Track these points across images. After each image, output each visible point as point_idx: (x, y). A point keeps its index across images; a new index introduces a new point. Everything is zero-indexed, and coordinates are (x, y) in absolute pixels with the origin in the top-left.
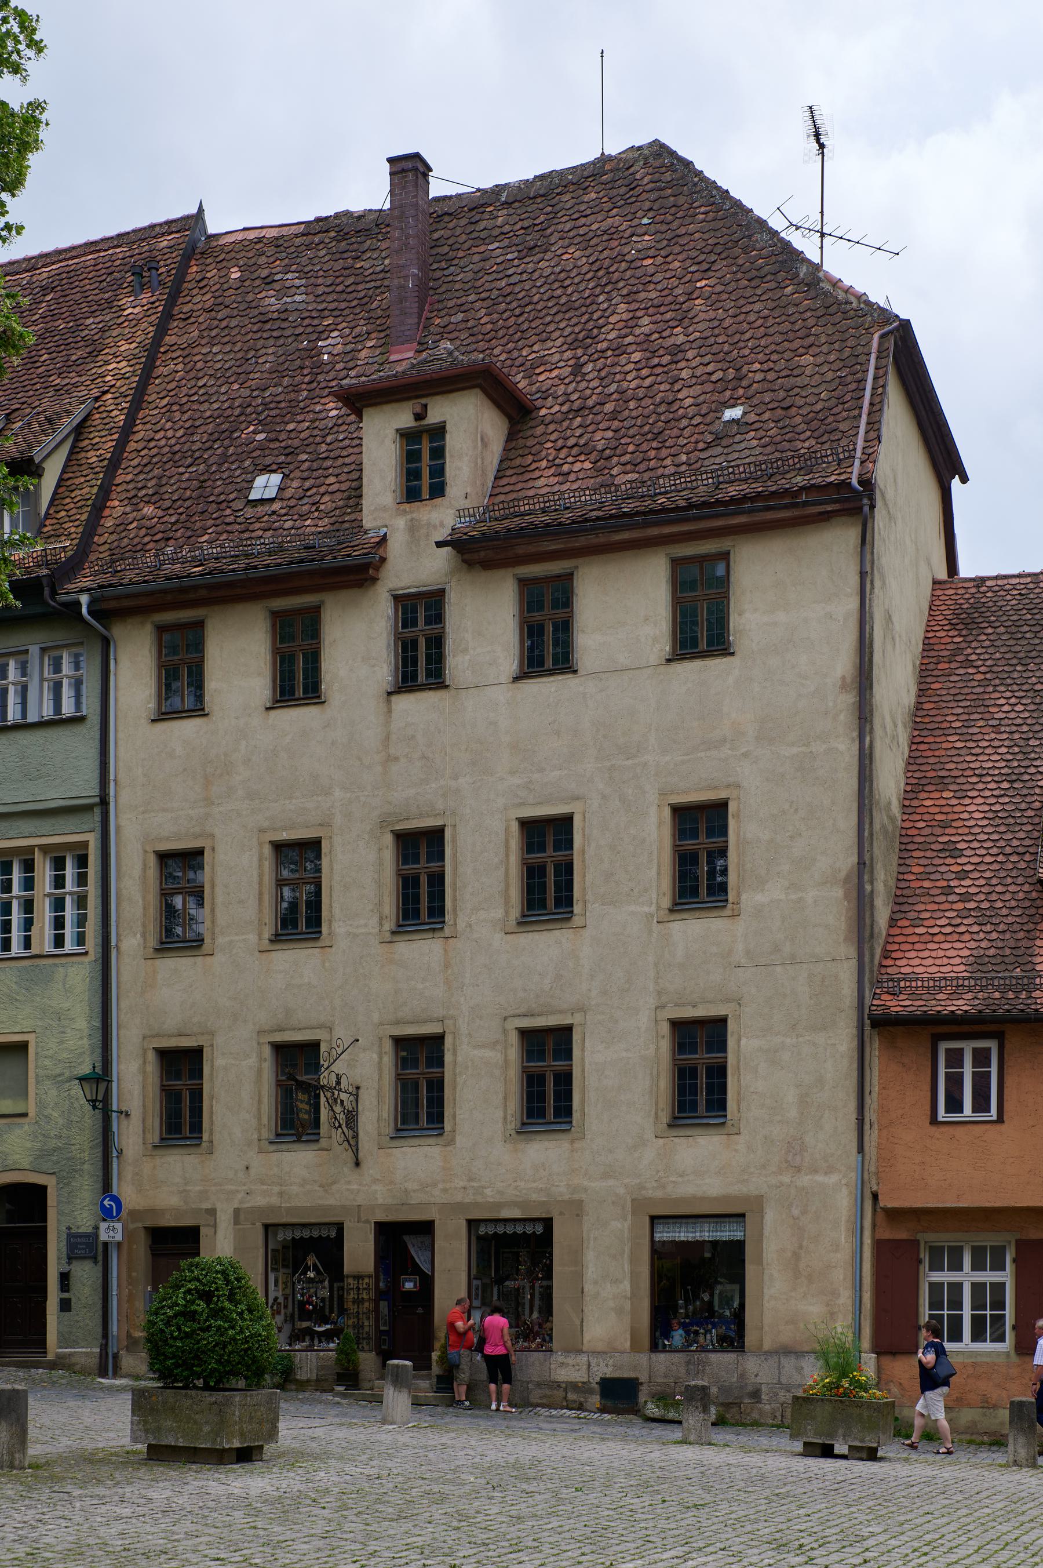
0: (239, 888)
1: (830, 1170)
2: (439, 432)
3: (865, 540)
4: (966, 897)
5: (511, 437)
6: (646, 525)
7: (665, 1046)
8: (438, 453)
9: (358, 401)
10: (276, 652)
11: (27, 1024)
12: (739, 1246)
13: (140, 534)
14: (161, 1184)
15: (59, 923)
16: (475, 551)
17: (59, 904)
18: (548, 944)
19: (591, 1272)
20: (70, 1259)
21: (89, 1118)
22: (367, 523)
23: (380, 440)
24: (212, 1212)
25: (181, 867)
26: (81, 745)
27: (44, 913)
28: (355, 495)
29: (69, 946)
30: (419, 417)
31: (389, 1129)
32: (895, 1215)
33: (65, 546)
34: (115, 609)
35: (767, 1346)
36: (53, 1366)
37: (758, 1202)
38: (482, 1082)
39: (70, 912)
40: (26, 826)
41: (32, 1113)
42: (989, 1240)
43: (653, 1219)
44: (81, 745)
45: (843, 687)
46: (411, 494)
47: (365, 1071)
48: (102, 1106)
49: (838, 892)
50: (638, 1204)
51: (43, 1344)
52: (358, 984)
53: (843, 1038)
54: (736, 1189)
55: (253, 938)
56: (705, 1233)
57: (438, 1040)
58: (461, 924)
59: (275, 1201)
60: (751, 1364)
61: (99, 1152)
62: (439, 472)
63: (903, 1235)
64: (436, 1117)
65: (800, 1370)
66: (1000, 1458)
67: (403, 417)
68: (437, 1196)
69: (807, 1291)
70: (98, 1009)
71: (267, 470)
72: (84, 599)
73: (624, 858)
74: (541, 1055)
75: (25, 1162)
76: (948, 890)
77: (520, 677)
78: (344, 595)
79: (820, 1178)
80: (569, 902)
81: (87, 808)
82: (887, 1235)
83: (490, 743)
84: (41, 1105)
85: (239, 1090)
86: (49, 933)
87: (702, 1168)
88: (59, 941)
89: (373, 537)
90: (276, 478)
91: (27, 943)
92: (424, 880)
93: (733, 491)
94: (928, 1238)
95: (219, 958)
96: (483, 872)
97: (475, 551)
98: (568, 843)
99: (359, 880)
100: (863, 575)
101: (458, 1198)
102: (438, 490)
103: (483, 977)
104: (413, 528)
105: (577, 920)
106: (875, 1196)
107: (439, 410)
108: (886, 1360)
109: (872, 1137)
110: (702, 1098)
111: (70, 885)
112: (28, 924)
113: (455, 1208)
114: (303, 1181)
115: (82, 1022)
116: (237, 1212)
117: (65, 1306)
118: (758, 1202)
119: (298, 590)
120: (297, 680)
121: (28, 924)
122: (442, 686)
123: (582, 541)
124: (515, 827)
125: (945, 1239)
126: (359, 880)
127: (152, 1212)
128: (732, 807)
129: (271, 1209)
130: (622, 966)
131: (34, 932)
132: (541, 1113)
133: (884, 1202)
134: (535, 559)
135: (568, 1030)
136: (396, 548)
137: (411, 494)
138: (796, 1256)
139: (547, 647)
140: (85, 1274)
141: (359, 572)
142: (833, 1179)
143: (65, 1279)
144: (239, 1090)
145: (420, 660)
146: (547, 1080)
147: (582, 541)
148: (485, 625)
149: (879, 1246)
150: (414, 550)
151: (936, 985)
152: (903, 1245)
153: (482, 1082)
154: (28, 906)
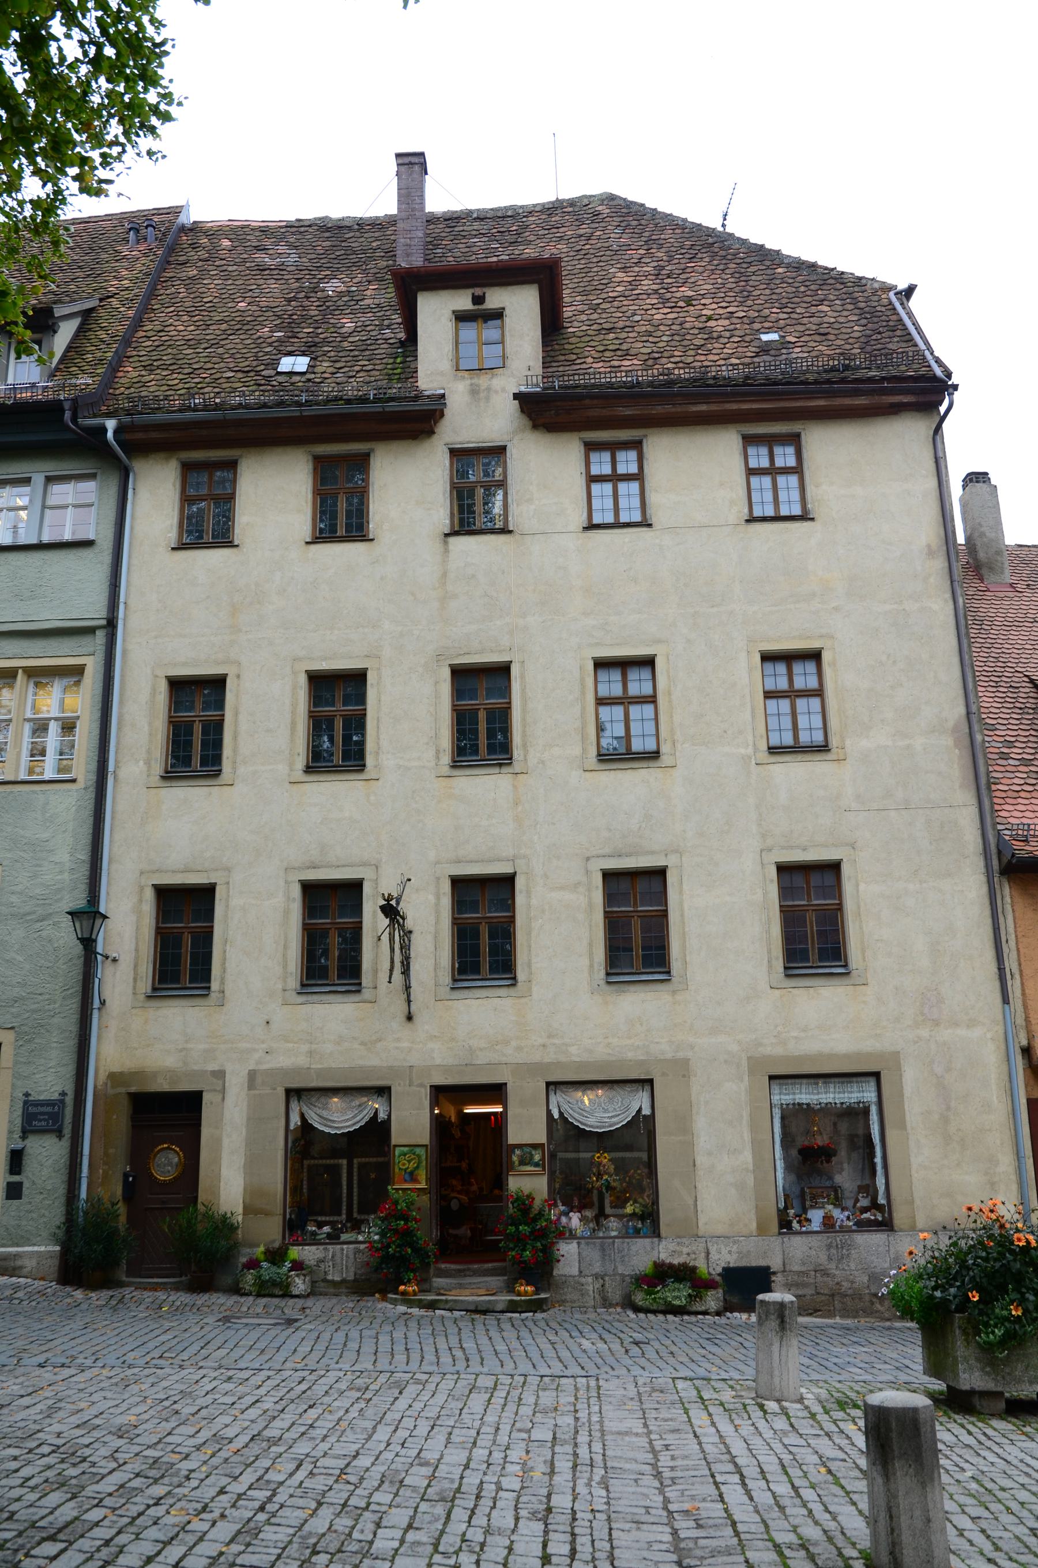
0: (265, 721)
1: (972, 1023)
2: (498, 315)
10: (317, 492)
12: (858, 1113)
13: (153, 384)
14: (147, 1038)
16: (545, 411)
19: (704, 1139)
20: (25, 1134)
22: (419, 384)
24: (220, 1074)
37: (895, 1059)
38: (560, 927)
43: (289, 1092)
45: (931, 553)
49: (948, 741)
50: (755, 1064)
52: (408, 823)
53: (968, 885)
54: (869, 1045)
55: (282, 768)
57: (509, 880)
58: (532, 761)
59: (302, 1061)
61: (74, 1005)
68: (510, 1055)
72: (111, 424)
73: (712, 700)
74: (474, 907)
78: (396, 446)
79: (962, 1032)
81: (91, 631)
85: (257, 937)
87: (823, 1021)
92: (198, 729)
101: (536, 1057)
103: (551, 822)
104: (474, 391)
105: (517, 766)
107: (496, 298)
113: (533, 1069)
114: (336, 1035)
115: (66, 854)
116: (252, 1075)
118: (895, 1059)
120: (341, 516)
127: (138, 1075)
129: (297, 1071)
138: (945, 1120)
141: (416, 420)
142: (977, 1033)
144: (257, 937)
146: (637, 925)
150: (482, 411)
153: (560, 927)
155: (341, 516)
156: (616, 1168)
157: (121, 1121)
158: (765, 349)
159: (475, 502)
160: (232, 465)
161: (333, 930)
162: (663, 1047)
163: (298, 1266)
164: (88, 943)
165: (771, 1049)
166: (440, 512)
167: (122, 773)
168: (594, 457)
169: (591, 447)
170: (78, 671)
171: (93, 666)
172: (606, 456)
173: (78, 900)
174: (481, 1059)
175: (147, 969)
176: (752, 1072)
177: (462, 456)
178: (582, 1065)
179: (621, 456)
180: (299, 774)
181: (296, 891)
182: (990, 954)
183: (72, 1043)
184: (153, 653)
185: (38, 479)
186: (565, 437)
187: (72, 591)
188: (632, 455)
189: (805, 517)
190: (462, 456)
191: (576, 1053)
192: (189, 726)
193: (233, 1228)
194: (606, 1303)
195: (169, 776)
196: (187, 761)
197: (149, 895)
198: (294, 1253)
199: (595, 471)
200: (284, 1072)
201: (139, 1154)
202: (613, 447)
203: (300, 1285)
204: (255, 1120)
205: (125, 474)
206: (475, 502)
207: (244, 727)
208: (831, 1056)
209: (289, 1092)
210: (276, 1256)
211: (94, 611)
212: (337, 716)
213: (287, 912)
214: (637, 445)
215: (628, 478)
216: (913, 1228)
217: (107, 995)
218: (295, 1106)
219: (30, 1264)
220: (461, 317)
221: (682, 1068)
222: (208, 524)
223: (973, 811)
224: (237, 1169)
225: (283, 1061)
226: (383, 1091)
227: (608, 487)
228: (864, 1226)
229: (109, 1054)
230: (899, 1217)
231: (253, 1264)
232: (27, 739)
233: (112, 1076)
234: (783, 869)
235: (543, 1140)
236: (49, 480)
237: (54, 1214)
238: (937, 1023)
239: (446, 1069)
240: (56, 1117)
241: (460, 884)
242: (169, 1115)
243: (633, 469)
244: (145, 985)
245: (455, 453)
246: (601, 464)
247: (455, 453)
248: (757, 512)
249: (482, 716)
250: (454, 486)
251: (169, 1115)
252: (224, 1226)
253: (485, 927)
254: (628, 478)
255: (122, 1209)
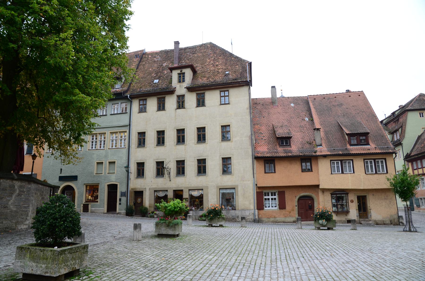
0: (151, 138)
1: (249, 181)
2: (184, 73)
3: (249, 88)
4: (265, 140)
5: (194, 75)
6: (217, 86)
7: (221, 162)
8: (184, 76)
9: (172, 69)
10: (158, 103)
11: (115, 159)
12: (233, 194)
13: (137, 87)
14: (136, 184)
15: (101, 144)
16: (190, 89)
17: (101, 142)
18: (201, 146)
19: (210, 197)
20: (121, 196)
21: (126, 173)
22: (173, 85)
23: (175, 74)
24: (145, 189)
25: (142, 135)
26: (127, 116)
27: (98, 143)
28: (171, 82)
29: (102, 148)
30: (181, 71)
31: (175, 175)
32: (259, 188)
33: (125, 88)
34: (133, 97)
35: (240, 209)
36: (118, 214)
37: (237, 186)
38: (191, 168)
39: (94, 143)
40: (117, 128)
41: (116, 172)
42: (273, 191)
43: (155, 191)
44: (127, 116)
45: (247, 109)
46: (180, 82)
47: (172, 166)
48: (128, 171)
49: (248, 138)
50: (217, 187)
51: (116, 210)
52: (170, 153)
53: (249, 160)
54: (234, 184)
55: (153, 145)
56: (228, 191)
57: (184, 161)
58: (187, 143)
59: (156, 187)
60: (237, 212)
61: (127, 179)
62: (184, 79)
63: (261, 191)
64: (183, 173)
65: (245, 213)
66: (296, 227)
67: (179, 71)
68: (184, 186)
69: (246, 201)
70: (127, 156)
71: (156, 79)
72: (129, 95)
73: (213, 134)
74: (201, 163)
75: (114, 180)
76: (262, 139)
77: (197, 107)
78: (169, 95)
79: (247, 182)
80: (164, 143)
81: (127, 126)
82: (258, 191)
83: (192, 116)
84: (117, 171)
85: (150, 169)
86: (99, 146)
87: (227, 181)
88: (112, 146)
89: (174, 87)
90: (158, 80)
91: (116, 146)
92: (181, 137)
93: (230, 82)
94: (265, 191)
95: (148, 148)
96: (191, 135)
97: (190, 89)
98: (164, 135)
99: (171, 137)
100: (249, 94)
101: (187, 186)
102: (184, 81)
103: (191, 151)
104: (180, 86)
105: (206, 142)
106: (256, 185)
107: (184, 71)
108: (259, 211)
109: (255, 175)
110: (202, 171)
111: (94, 140)
112: (96, 145)
113: (187, 188)
114: (161, 183)
115: (125, 158)
116: (150, 188)
117: (120, 204)
118: (237, 186)
119: (162, 94)
120: (161, 107)
121: (96, 145)
122: (184, 108)
123: (207, 88)
124: (196, 129)
125: (267, 191)
126: (171, 137)
127: (135, 189)
128: (185, 130)
129: (155, 188)
130: (213, 150)
131: (117, 145)
132: (159, 174)
133: (258, 185)
134: (199, 90)
135: (205, 159)
136: (177, 89)
137: (180, 82)
138: (244, 195)
139: (201, 103)
140: (124, 199)
141: (172, 92)
142: (249, 182)
143: (120, 200)
144: (150, 169)
145: (181, 104)
146: (202, 167)
147: (207, 88)
148: (191, 99)
149: (257, 192)
150: (181, 89)
151: (263, 153)
152: (261, 193)
153: (191, 168)
154: (96, 142)
155: (161, 107)
156: (197, 201)
157: (133, 195)
158: (226, 75)
159: (181, 104)
160: (164, 98)
161: (160, 168)
162: (205, 185)
163: (155, 214)
164: (128, 171)
165: (220, 184)
166: (175, 106)
167: (132, 147)
168: (221, 93)
169: (221, 91)
170: (126, 132)
171: (128, 131)
172: (223, 93)
173: (126, 165)
174: (180, 186)
175: (136, 174)
176: (217, 188)
177: (178, 97)
178: (194, 187)
179: (226, 92)
180: (221, 141)
181: (155, 163)
182: (252, 171)
183: (126, 184)
184: (135, 130)
185: (120, 103)
186: (193, 93)
187: (124, 120)
188: (227, 92)
189: (229, 104)
190: (178, 97)
191: (193, 185)
192: (180, 136)
193: (147, 209)
194: (196, 219)
195: (138, 147)
196: (200, 140)
197: (136, 164)
198: (155, 212)
199: (222, 95)
200: (154, 188)
201: (136, 199)
202: (224, 91)
203: (155, 216)
204: (150, 195)
205: (131, 102)
206: (181, 104)
207: (148, 139)
208: (227, 186)
209: (155, 191)
210: (153, 212)
211: (128, 123)
212: (161, 138)
213: (195, 165)
214: (228, 91)
215: (227, 96)
216: (238, 210)
217: (131, 178)
218: (156, 193)
219: (122, 213)
220: (179, 74)
221: (207, 187)
222: (143, 110)
223: (251, 149)
224: (148, 201)
225: (154, 187)
226: (167, 191)
227: (224, 98)
228: (233, 209)
229: (131, 186)
230: (237, 208)
231: (150, 214)
232: (120, 142)
233: (132, 189)
234: (223, 158)
235: (188, 197)
236: (121, 103)
237: (125, 207)
238: (244, 181)
239: (175, 188)
240: (125, 194)
241: (177, 161)
242: (139, 194)
243: (227, 95)
244: (136, 176)
245: (177, 96)
246: (222, 94)
247: (177, 96)
248: (222, 103)
249: (201, 135)
250: (177, 101)
251: (139, 194)
252: (146, 209)
253: (181, 167)
254: (227, 96)
255: (134, 206)
